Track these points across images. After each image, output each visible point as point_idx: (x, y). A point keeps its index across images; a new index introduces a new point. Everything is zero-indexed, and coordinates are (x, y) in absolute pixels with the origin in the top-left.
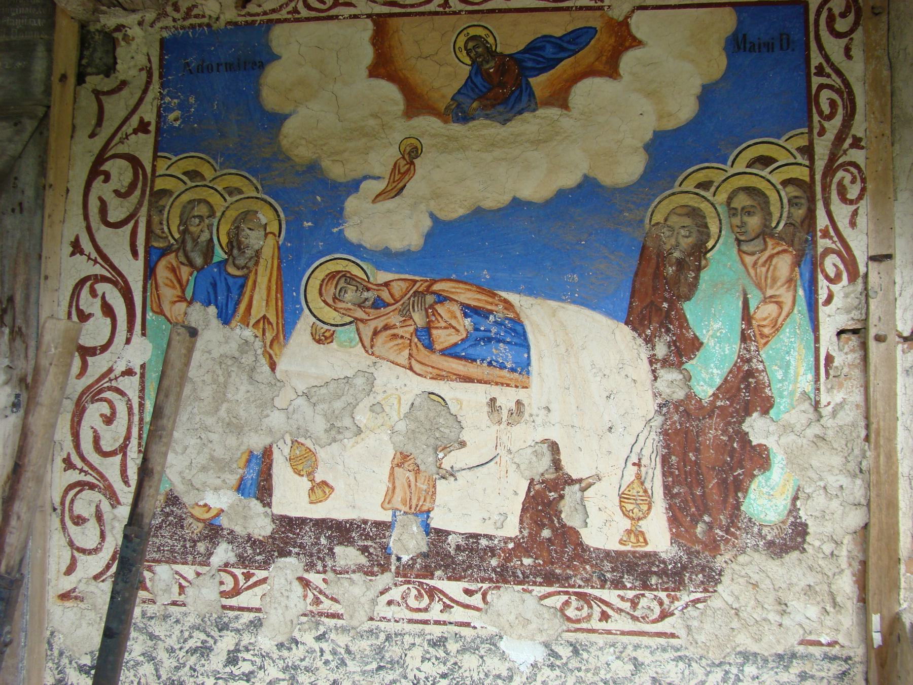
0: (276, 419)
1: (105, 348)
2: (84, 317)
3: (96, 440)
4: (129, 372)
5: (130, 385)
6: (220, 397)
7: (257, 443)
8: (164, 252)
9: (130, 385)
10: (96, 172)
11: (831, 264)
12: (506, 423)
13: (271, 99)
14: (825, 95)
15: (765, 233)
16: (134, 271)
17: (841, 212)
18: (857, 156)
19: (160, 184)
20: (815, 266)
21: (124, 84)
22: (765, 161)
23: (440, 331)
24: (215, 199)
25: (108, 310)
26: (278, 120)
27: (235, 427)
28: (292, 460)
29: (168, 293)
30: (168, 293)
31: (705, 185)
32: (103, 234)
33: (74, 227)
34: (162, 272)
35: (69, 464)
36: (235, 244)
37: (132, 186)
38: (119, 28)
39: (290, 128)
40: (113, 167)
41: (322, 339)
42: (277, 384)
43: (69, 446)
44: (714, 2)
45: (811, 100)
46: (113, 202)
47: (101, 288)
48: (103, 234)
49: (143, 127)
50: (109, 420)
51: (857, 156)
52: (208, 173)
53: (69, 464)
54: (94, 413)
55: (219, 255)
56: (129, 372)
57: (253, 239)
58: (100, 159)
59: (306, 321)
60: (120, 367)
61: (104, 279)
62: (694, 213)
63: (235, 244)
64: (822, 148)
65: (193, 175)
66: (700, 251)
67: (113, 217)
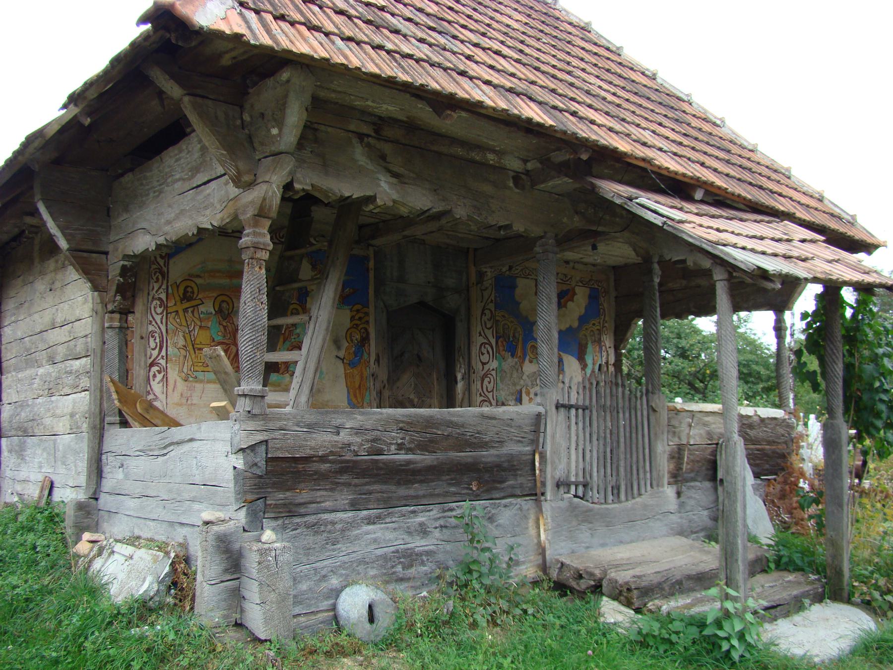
0: (522, 382)
1: (488, 363)
2: (483, 354)
3: (487, 388)
4: (493, 370)
5: (493, 373)
6: (511, 377)
7: (518, 388)
8: (500, 337)
9: (493, 373)
10: (483, 313)
11: (604, 348)
12: (554, 408)
13: (517, 298)
14: (602, 310)
15: (595, 341)
16: (493, 342)
17: (605, 336)
18: (606, 325)
19: (497, 318)
20: (602, 349)
21: (487, 288)
22: (594, 324)
23: (47, 419)
24: (509, 324)
25: (488, 352)
26: (518, 304)
27: (514, 384)
28: (526, 392)
29: (501, 348)
30: (501, 348)
31: (586, 329)
32: (486, 331)
33: (479, 329)
34: (500, 343)
35: (481, 395)
36: (514, 336)
37: (491, 318)
38: (486, 272)
39: (521, 306)
40: (487, 312)
41: (531, 362)
42: (522, 373)
43: (480, 390)
44: (633, 53)
45: (600, 311)
46: (488, 322)
47: (487, 346)
48: (486, 331)
49: (492, 301)
50: (489, 383)
51: (606, 325)
52: (506, 316)
53: (481, 395)
54: (487, 380)
55: (511, 339)
56: (493, 370)
57: (517, 335)
58: (483, 310)
59: (528, 358)
60: (491, 368)
61: (487, 344)
62: (585, 336)
63: (514, 336)
64: (602, 321)
65: (504, 316)
66: (587, 344)
67: (488, 326)
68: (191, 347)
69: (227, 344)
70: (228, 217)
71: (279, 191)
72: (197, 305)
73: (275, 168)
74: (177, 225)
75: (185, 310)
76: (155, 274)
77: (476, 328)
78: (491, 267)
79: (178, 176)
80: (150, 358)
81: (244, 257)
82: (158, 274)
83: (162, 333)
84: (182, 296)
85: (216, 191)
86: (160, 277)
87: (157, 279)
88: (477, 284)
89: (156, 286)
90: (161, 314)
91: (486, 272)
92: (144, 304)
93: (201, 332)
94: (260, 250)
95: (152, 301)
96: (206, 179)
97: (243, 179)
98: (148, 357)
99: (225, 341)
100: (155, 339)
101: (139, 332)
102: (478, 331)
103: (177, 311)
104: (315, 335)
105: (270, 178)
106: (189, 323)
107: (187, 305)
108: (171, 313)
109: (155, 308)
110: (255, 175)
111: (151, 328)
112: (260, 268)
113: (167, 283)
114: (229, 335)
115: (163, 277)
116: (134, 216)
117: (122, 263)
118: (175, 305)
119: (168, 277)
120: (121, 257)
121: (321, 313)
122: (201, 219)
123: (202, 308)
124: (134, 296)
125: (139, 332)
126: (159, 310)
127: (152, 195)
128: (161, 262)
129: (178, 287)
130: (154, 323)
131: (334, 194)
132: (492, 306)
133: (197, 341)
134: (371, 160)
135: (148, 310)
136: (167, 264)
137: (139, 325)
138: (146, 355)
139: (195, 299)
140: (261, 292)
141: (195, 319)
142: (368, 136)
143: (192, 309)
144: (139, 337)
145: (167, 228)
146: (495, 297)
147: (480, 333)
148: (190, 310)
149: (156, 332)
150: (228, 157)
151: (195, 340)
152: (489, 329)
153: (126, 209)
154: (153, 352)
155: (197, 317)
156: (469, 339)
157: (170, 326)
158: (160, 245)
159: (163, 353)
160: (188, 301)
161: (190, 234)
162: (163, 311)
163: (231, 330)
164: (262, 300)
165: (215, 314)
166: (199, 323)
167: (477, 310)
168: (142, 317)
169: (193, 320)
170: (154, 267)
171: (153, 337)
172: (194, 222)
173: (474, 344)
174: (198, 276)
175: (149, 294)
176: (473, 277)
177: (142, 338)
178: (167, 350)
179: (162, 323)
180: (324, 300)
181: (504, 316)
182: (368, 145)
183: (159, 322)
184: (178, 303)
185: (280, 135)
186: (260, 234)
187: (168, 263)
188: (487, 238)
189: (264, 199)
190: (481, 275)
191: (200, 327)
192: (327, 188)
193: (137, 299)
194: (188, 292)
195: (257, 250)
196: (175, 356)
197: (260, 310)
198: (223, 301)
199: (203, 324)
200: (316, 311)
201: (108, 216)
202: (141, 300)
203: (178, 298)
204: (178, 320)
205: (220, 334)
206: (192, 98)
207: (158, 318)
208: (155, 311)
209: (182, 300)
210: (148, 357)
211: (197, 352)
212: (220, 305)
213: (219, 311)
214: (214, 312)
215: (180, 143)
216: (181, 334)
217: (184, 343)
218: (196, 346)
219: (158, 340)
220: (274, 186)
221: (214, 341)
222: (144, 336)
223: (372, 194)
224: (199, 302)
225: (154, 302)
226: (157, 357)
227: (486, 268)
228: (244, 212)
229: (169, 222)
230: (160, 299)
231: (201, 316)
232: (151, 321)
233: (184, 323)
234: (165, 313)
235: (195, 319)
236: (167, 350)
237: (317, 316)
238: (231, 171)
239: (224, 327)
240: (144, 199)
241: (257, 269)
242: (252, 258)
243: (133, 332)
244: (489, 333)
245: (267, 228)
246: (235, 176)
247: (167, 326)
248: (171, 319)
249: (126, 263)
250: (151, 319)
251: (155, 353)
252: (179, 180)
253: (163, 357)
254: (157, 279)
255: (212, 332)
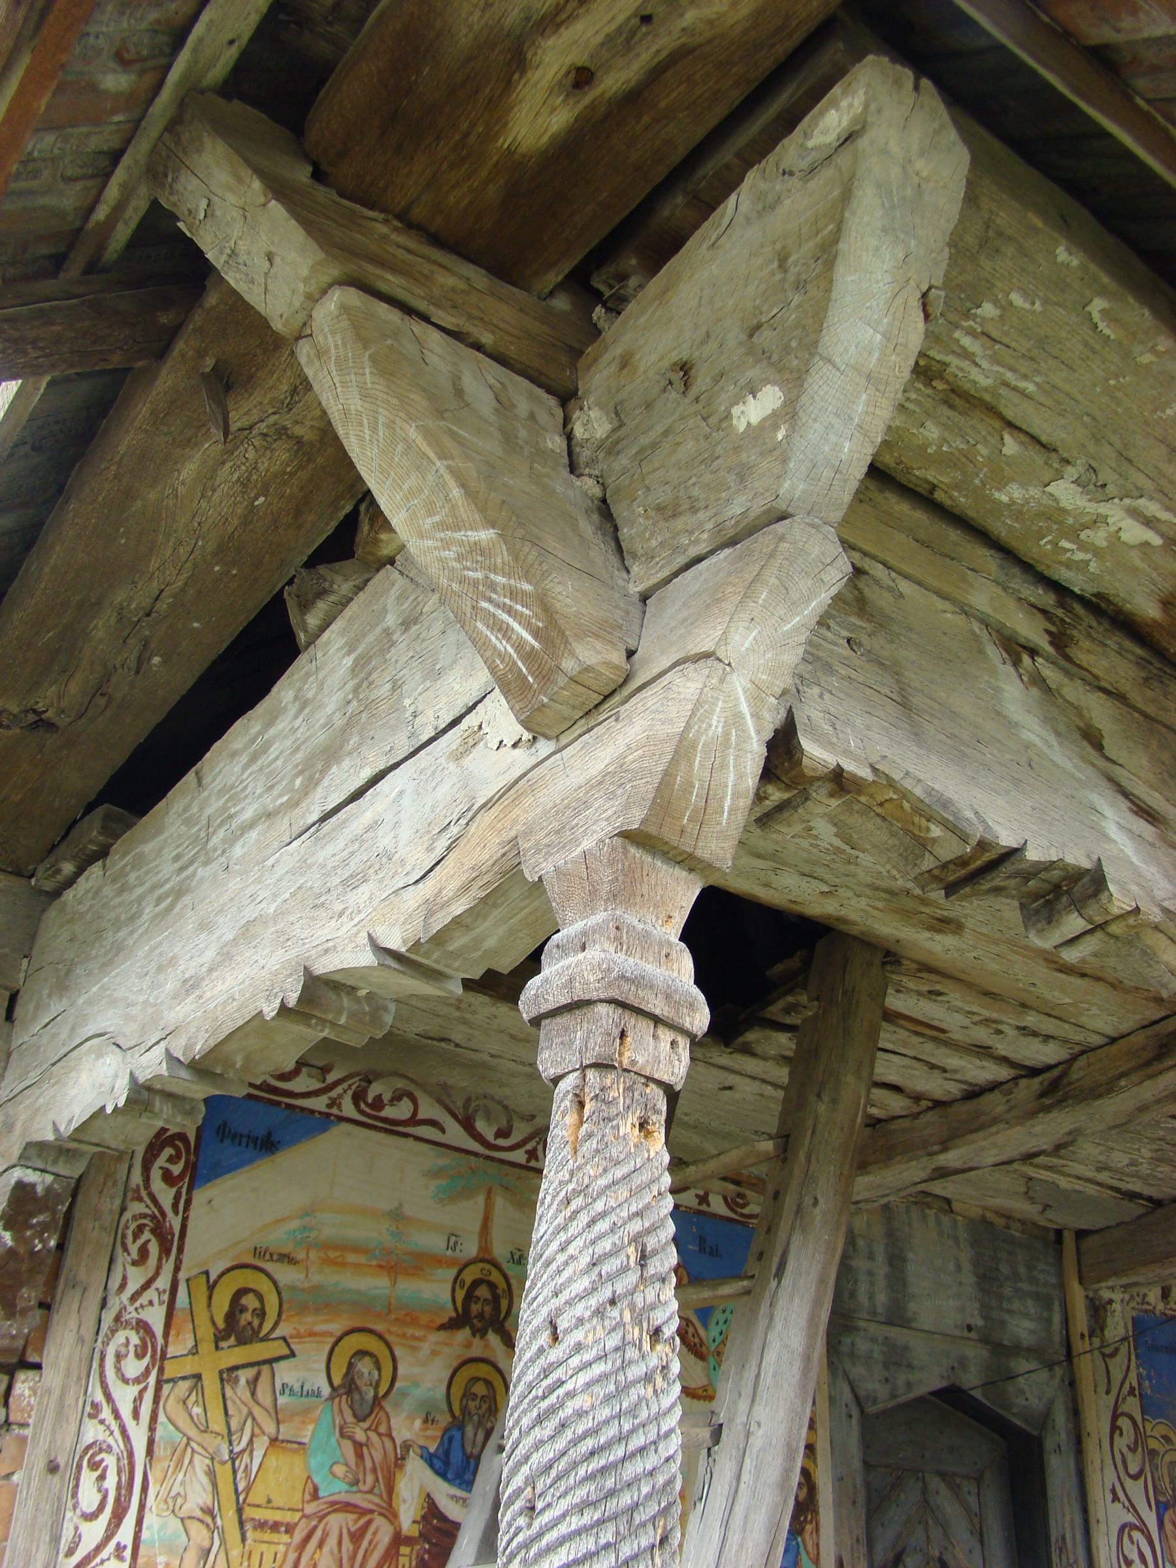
10: (1114, 1428)
16: (1151, 1519)
19: (1153, 1444)
33: (1110, 1477)
37: (1136, 1442)
38: (1110, 1301)
40: (1123, 1422)
46: (1129, 1456)
48: (1129, 1483)
58: (1115, 1417)
61: (1134, 1527)
68: (231, 1514)
69: (364, 1512)
70: (465, 888)
71: (756, 716)
72: (270, 1362)
73: (749, 593)
74: (220, 987)
75: (228, 1375)
76: (136, 1236)
77: (1102, 1478)
78: (1125, 1287)
79: (248, 814)
80: (70, 1552)
81: (547, 1064)
82: (147, 1235)
83: (131, 1454)
84: (221, 1325)
85: (406, 801)
86: (154, 1248)
87: (144, 1252)
88: (1091, 1334)
89: (136, 1278)
90: (137, 1381)
91: (1110, 1301)
92: (81, 1340)
93: (272, 1461)
94: (645, 1026)
95: (113, 1332)
96: (366, 774)
97: (568, 665)
98: (63, 1547)
99: (356, 1499)
100: (102, 1477)
101: (43, 1444)
102: (1108, 1486)
103: (198, 1377)
104: (739, 1510)
105: (724, 638)
106: (234, 1424)
107: (234, 1355)
108: (173, 1380)
109: (119, 1357)
110: (630, 654)
111: (92, 1432)
112: (643, 1125)
113: (177, 1269)
114: (370, 1478)
115: (165, 1250)
116: (81, 1001)
117: (17, 1174)
118: (194, 1351)
119: (181, 1250)
120: (16, 1151)
121: (760, 1412)
122: (326, 931)
123: (286, 1373)
124: (46, 1306)
125: (43, 1444)
126: (133, 1367)
127: (148, 911)
128: (165, 1195)
129: (211, 1288)
130: (106, 1413)
131: (954, 829)
132: (1132, 1405)
133: (257, 1496)
134: (1058, 734)
135: (93, 1361)
136: (183, 1205)
137: (50, 1415)
138: (56, 1539)
139: (266, 1339)
140: (652, 1269)
141: (257, 1411)
142: (1033, 652)
143: (250, 1373)
144: (41, 1464)
145: (183, 1011)
146: (1139, 1376)
147: (1113, 1491)
148: (244, 1376)
149: (109, 1449)
150: (502, 556)
151: (248, 1489)
152: (1135, 1477)
153: (63, 986)
154: (85, 1528)
155: (268, 1401)
156: (1085, 1510)
157: (164, 1429)
158: (148, 1088)
159: (125, 1534)
160: (241, 1342)
161: (270, 1010)
162: (147, 1372)
163: (378, 1457)
164: (659, 1317)
165: (331, 1398)
166: (270, 1427)
167: (1097, 1421)
168: (64, 1390)
169: (250, 1413)
170: (136, 1208)
171: (94, 1466)
172: (293, 953)
173: (1103, 1527)
174: (286, 1258)
175: (104, 1304)
176: (1081, 1321)
177: (53, 1468)
178: (139, 1522)
179: (136, 1414)
180: (770, 1357)
181: (1166, 1438)
182: (1038, 680)
183: (126, 1411)
184: (207, 1347)
185: (789, 413)
186: (643, 943)
187: (188, 1202)
188: (1132, 1196)
189: (683, 749)
190: (1098, 1310)
191: (274, 1441)
192: (930, 791)
193: (56, 1318)
194: (243, 1309)
195: (630, 1020)
196: (169, 1548)
197: (648, 1378)
198: (362, 1353)
199: (285, 1432)
200: (743, 1405)
201: (9, 1016)
202: (73, 1324)
203: (206, 1332)
204: (197, 1410)
205: (340, 1470)
206: (353, 297)
207: (124, 1396)
208: (118, 1369)
209: (220, 1337)
210: (63, 1547)
211: (250, 1534)
212: (350, 1366)
213: (348, 1387)
214: (326, 1391)
215: (275, 689)
216: (201, 1463)
217: (204, 1498)
218: (249, 1512)
219: (111, 1482)
220: (739, 684)
221: (315, 1496)
222: (61, 1461)
223: (1086, 864)
224: (279, 1349)
225: (120, 1337)
226: (98, 1549)
227: (1112, 1288)
228: (563, 834)
229: (190, 985)
230: (143, 1326)
231: (282, 1400)
232: (96, 1407)
233: (218, 1424)
234: (152, 1380)
235: (257, 1411)
236: (139, 1522)
237: (747, 1425)
238: (505, 631)
239: (358, 1447)
240: (121, 934)
241: (628, 1127)
242: (602, 1066)
243: (23, 1440)
244: (1135, 1489)
245: (680, 919)
246: (529, 656)
247: (152, 1429)
248: (171, 1404)
249: (31, 1177)
250: (99, 1397)
251: (93, 1532)
252: (251, 825)
253: (120, 1548)
254: (144, 1252)
255: (314, 1462)
